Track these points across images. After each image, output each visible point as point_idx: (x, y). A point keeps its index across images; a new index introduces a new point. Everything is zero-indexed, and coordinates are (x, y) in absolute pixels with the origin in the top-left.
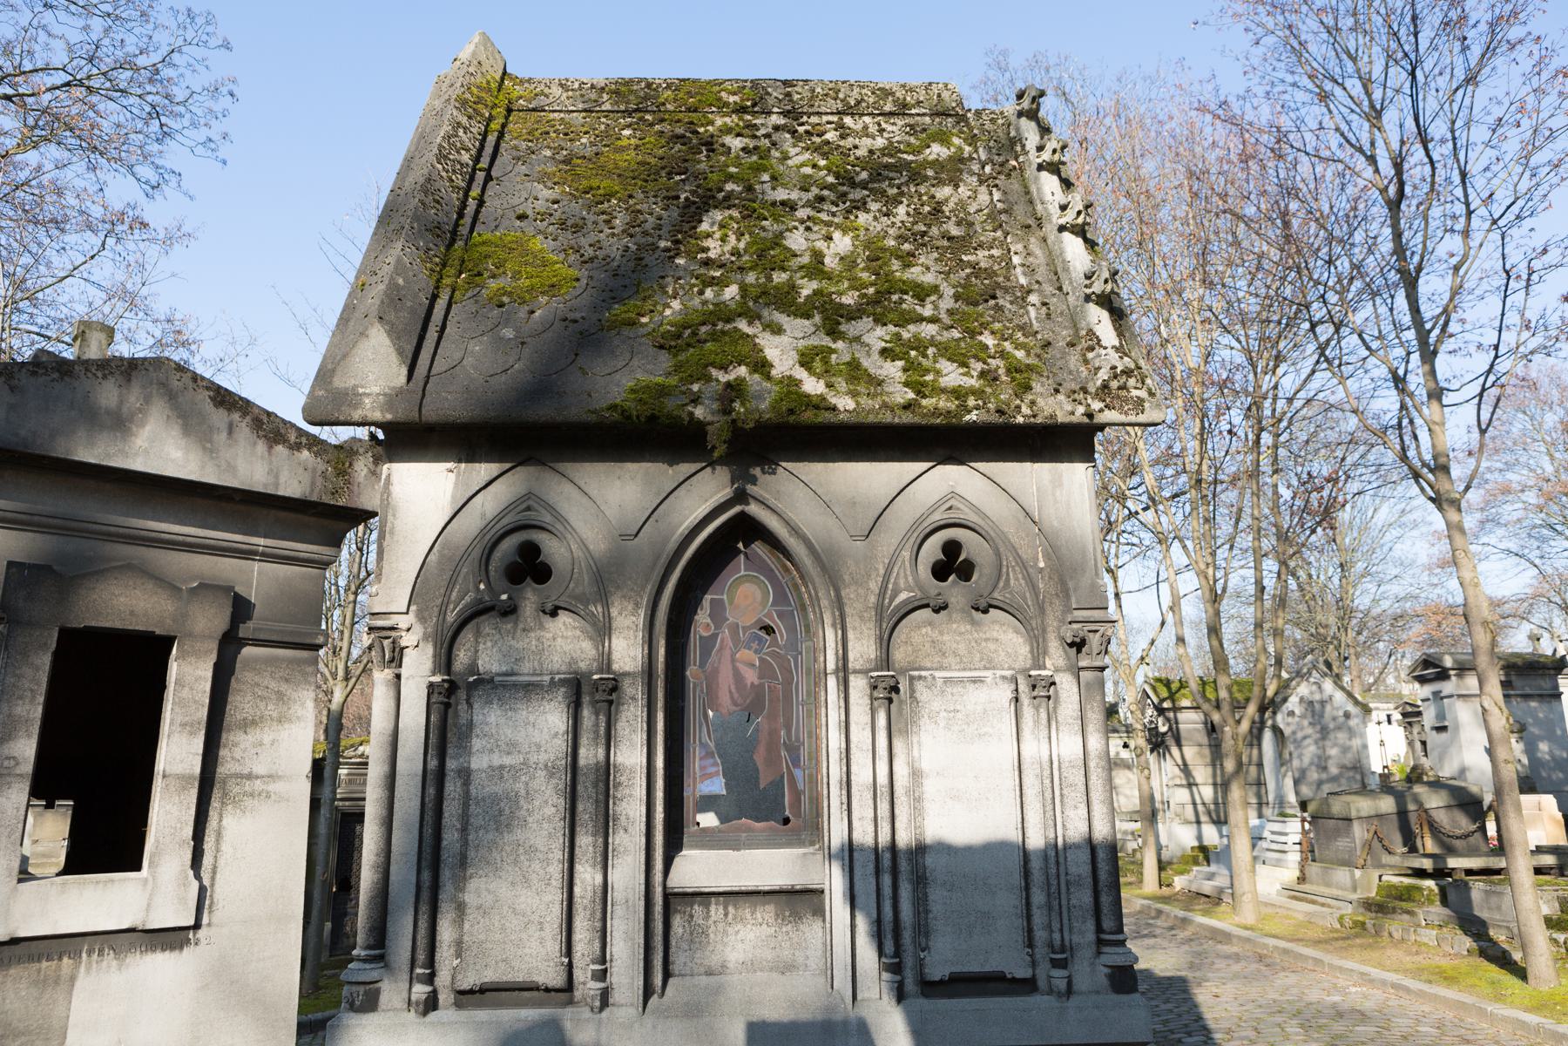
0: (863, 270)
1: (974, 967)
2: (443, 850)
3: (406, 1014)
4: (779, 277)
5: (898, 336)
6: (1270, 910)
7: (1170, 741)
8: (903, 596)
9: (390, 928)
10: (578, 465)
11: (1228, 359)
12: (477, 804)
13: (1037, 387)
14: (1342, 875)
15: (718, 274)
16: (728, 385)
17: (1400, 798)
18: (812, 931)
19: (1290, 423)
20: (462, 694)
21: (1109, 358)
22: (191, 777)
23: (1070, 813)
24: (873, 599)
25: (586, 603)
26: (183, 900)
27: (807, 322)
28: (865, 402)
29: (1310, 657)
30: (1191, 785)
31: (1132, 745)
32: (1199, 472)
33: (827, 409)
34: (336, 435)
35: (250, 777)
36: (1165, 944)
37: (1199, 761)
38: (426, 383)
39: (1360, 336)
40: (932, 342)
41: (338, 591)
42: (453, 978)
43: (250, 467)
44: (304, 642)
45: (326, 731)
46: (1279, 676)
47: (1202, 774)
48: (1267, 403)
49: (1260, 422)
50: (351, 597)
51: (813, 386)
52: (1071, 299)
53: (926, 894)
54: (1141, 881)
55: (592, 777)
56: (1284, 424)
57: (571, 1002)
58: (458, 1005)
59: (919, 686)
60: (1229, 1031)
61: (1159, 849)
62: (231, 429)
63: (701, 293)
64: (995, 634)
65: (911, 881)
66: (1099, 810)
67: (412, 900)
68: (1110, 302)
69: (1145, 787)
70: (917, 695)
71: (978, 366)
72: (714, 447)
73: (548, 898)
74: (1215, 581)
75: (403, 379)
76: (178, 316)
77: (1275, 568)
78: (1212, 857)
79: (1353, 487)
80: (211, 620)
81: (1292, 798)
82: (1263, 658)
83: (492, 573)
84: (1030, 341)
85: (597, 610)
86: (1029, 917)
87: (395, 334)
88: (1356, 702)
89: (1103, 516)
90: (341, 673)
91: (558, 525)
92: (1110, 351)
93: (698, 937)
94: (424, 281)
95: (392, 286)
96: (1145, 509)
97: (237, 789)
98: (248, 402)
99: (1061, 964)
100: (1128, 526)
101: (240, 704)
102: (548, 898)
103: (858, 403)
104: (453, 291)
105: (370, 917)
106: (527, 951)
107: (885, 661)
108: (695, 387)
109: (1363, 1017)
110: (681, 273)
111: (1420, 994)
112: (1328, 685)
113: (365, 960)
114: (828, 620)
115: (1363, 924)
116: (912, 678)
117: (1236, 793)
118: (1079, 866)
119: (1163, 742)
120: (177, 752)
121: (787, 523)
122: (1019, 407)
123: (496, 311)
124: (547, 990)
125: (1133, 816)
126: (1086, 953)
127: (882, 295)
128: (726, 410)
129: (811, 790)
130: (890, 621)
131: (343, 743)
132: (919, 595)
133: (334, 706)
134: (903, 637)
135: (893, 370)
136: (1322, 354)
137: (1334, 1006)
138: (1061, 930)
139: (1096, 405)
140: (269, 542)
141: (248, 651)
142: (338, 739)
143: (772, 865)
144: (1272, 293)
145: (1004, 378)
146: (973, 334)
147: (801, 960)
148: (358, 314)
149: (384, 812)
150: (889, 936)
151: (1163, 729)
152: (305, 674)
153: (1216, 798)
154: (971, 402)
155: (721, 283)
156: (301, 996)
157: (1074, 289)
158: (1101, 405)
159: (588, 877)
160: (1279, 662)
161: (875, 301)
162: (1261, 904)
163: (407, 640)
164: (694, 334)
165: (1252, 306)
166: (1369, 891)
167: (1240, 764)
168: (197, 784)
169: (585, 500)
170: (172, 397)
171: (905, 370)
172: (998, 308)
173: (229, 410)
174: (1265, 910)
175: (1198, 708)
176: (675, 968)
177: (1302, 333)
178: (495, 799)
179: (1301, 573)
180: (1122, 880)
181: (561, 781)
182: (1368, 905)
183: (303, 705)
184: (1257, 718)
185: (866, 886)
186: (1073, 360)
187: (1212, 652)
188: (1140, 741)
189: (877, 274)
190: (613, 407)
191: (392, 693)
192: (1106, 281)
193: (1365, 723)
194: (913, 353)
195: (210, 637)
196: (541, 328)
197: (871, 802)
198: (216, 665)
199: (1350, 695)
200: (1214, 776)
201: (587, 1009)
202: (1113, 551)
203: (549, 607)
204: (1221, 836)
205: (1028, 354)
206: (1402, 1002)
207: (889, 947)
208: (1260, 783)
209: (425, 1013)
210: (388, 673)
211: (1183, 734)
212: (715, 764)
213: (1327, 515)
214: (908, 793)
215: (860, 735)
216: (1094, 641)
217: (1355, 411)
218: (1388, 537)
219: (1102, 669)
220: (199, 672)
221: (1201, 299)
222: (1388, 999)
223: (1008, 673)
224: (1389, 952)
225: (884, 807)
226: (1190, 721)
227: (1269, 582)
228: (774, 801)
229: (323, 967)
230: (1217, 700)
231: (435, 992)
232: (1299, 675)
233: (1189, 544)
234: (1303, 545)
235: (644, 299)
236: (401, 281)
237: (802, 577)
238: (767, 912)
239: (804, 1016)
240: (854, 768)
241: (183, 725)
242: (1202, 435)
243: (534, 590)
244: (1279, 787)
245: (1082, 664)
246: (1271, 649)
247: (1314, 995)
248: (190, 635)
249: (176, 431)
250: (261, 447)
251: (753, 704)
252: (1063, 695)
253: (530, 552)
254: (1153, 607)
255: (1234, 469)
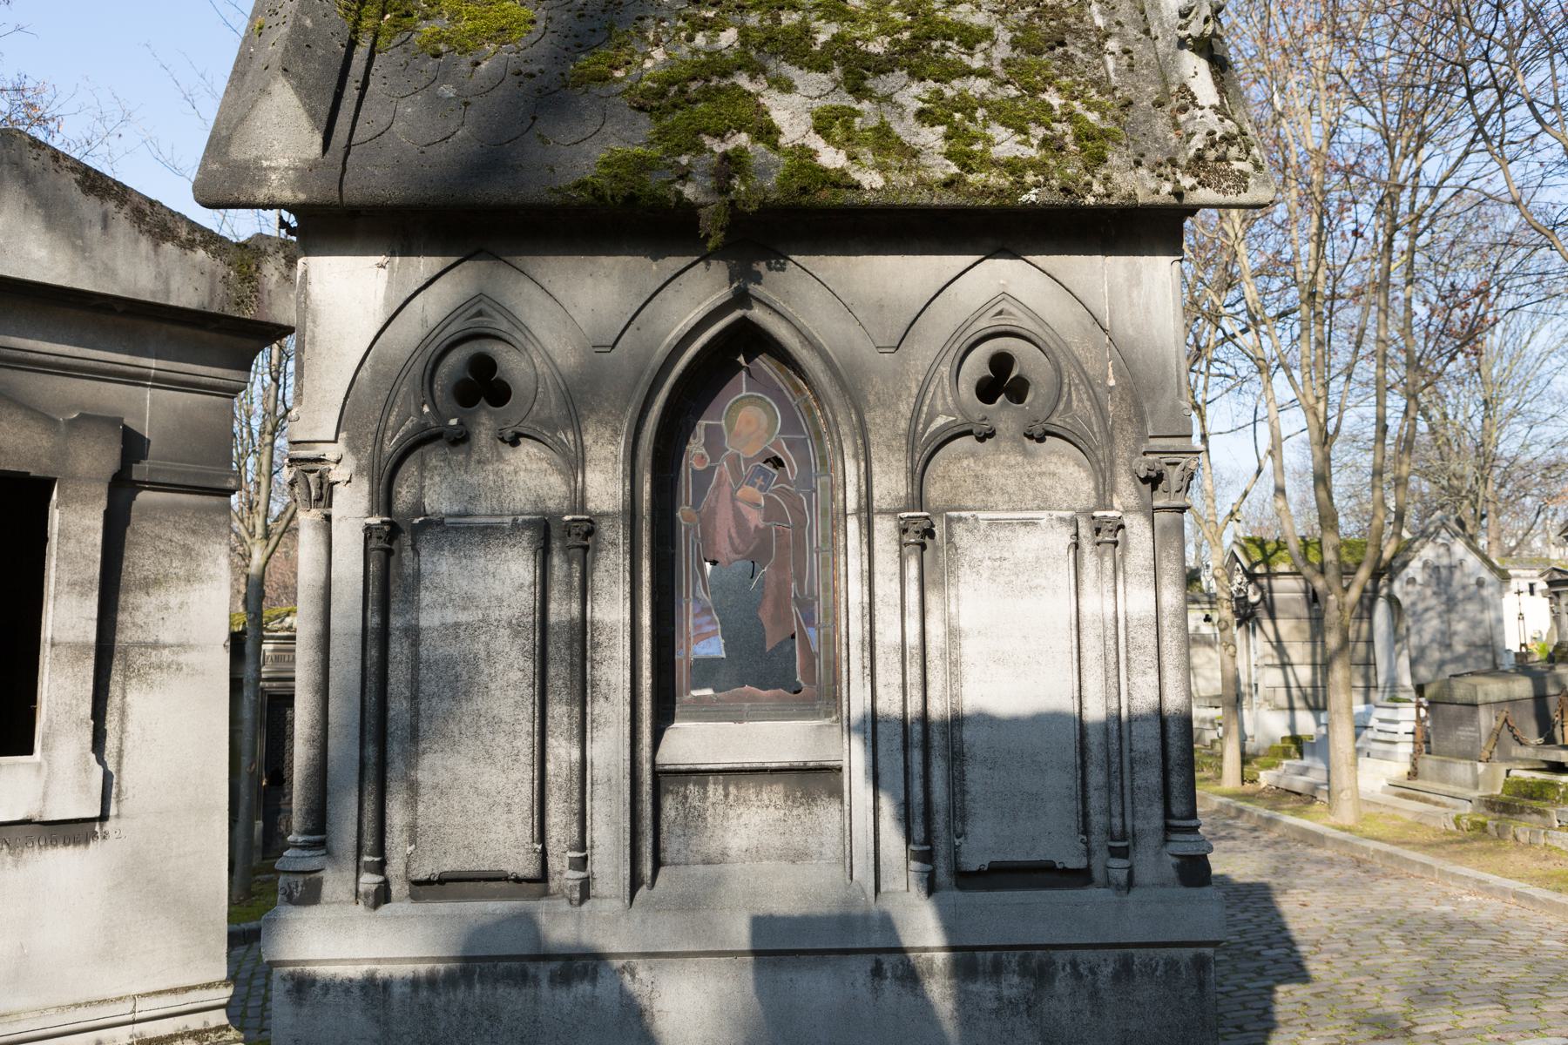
0: (896, 8)
1: (1018, 855)
2: (392, 717)
3: (353, 906)
4: (789, 19)
5: (939, 94)
6: (1373, 810)
7: (1262, 613)
8: (941, 421)
9: (332, 810)
10: (538, 259)
11: (1357, 139)
12: (429, 667)
13: (1113, 159)
14: (1462, 770)
15: (711, 14)
16: (725, 156)
17: (1538, 680)
18: (827, 814)
19: (1433, 219)
20: (406, 539)
21: (1204, 122)
22: (85, 646)
23: (1137, 679)
24: (903, 424)
25: (554, 430)
26: (85, 788)
27: (824, 77)
28: (898, 179)
29: (1439, 513)
30: (1285, 665)
31: (1215, 619)
32: (1313, 283)
33: (849, 187)
34: (241, 225)
35: (156, 645)
36: (1246, 846)
37: (1296, 636)
38: (347, 154)
39: (1530, 104)
40: (982, 102)
41: (251, 434)
42: (407, 866)
43: (133, 270)
44: (210, 482)
45: (245, 602)
46: (1399, 535)
47: (1299, 652)
48: (1405, 197)
49: (1394, 219)
50: (268, 439)
51: (831, 158)
52: (1160, 45)
53: (963, 773)
54: (1220, 777)
55: (565, 636)
56: (1425, 222)
57: (545, 894)
58: (414, 897)
59: (959, 529)
60: (1317, 943)
61: (1243, 739)
62: (105, 222)
63: (690, 39)
64: (1052, 467)
65: (945, 757)
66: (1172, 677)
67: (356, 778)
68: (1211, 48)
69: (1229, 667)
70: (956, 540)
71: (1039, 132)
72: (708, 236)
73: (516, 776)
74: (1327, 420)
75: (317, 149)
76: (29, 84)
77: (1402, 404)
78: (1306, 748)
79: (1508, 301)
80: (96, 459)
81: (1406, 681)
82: (1381, 513)
83: (438, 393)
84: (1106, 100)
85: (568, 437)
86: (1084, 799)
87: (304, 91)
88: (1493, 568)
89: (1191, 340)
90: (259, 530)
91: (515, 334)
92: (1207, 111)
93: (693, 821)
94: (339, 24)
95: (298, 28)
96: (1244, 331)
97: (141, 661)
98: (125, 187)
99: (1122, 853)
100: (1220, 353)
101: (139, 560)
102: (516, 776)
103: (887, 180)
104: (376, 37)
105: (306, 798)
106: (492, 836)
107: (918, 498)
108: (684, 160)
109: (1477, 928)
110: (665, 14)
111: (1547, 904)
112: (1459, 547)
113: (303, 847)
114: (848, 450)
115: (1484, 825)
116: (950, 520)
117: (1339, 673)
118: (1146, 741)
119: (1253, 614)
120: (67, 616)
121: (799, 331)
122: (1089, 184)
123: (431, 63)
124: (518, 880)
125: (1212, 702)
126: (1150, 842)
127: (920, 41)
128: (723, 189)
129: (827, 652)
130: (924, 453)
131: (266, 613)
132: (960, 419)
133: (254, 569)
134: (940, 471)
135: (932, 138)
136: (1480, 130)
137: (1443, 916)
138: (1123, 815)
139: (1187, 181)
140: (162, 364)
141: (144, 497)
142: (260, 607)
143: (781, 739)
144: (1420, 49)
145: (1072, 147)
146: (1034, 90)
147: (814, 847)
148: (257, 65)
149: (318, 678)
150: (919, 820)
151: (1254, 598)
152: (215, 525)
153: (1314, 681)
154: (1030, 178)
155: (714, 26)
156: (231, 904)
157: (1165, 31)
158: (1194, 181)
159: (562, 751)
160: (1400, 517)
161: (912, 49)
162: (1362, 802)
163: (338, 474)
164: (682, 92)
165: (1393, 66)
166: (1493, 787)
167: (1345, 641)
168: (92, 654)
169: (549, 302)
170: (28, 180)
171: (947, 137)
172: (1067, 58)
173: (102, 198)
174: (1366, 810)
175: (1299, 573)
176: (667, 856)
177: (1456, 100)
178: (450, 662)
179: (1435, 413)
180: (1198, 775)
181: (528, 641)
182: (1491, 804)
183: (215, 561)
184: (1369, 585)
185: (892, 764)
186: (1161, 124)
187: (1319, 507)
188: (1225, 612)
189: (914, 14)
190: (581, 185)
191: (321, 538)
192: (1206, 21)
193: (1501, 593)
194: (958, 116)
195: (98, 480)
196: (489, 85)
197: (898, 666)
198: (107, 514)
199: (1486, 559)
200: (1314, 653)
201: (565, 902)
202: (1201, 383)
203: (508, 434)
204: (1319, 724)
205: (1103, 117)
206: (1525, 913)
207: (919, 832)
208: (1369, 663)
209: (376, 906)
210: (315, 514)
211: (1278, 605)
212: (712, 622)
213: (1471, 336)
214: (942, 656)
215: (886, 587)
216: (1174, 475)
217: (1516, 203)
218: (1547, 366)
219: (1182, 510)
220: (87, 522)
221: (1328, 58)
222: (1508, 910)
223: (1067, 514)
224: (1512, 857)
225: (914, 672)
226: (1287, 589)
227: (1394, 422)
228: (782, 663)
229: (256, 871)
230: (1322, 564)
231: (386, 883)
232: (1424, 535)
233: (1297, 374)
234: (1439, 374)
235: (618, 47)
236: (308, 22)
237: (817, 399)
238: (774, 792)
239: (820, 909)
240: (878, 626)
241: (72, 585)
242: (1319, 235)
243: (489, 413)
244: (1392, 668)
245: (1158, 503)
246: (1391, 504)
247: (1420, 905)
248: (73, 477)
249: (37, 225)
250: (145, 244)
251: (758, 552)
252: (1133, 541)
253: (484, 367)
254: (1248, 451)
255: (1356, 281)
